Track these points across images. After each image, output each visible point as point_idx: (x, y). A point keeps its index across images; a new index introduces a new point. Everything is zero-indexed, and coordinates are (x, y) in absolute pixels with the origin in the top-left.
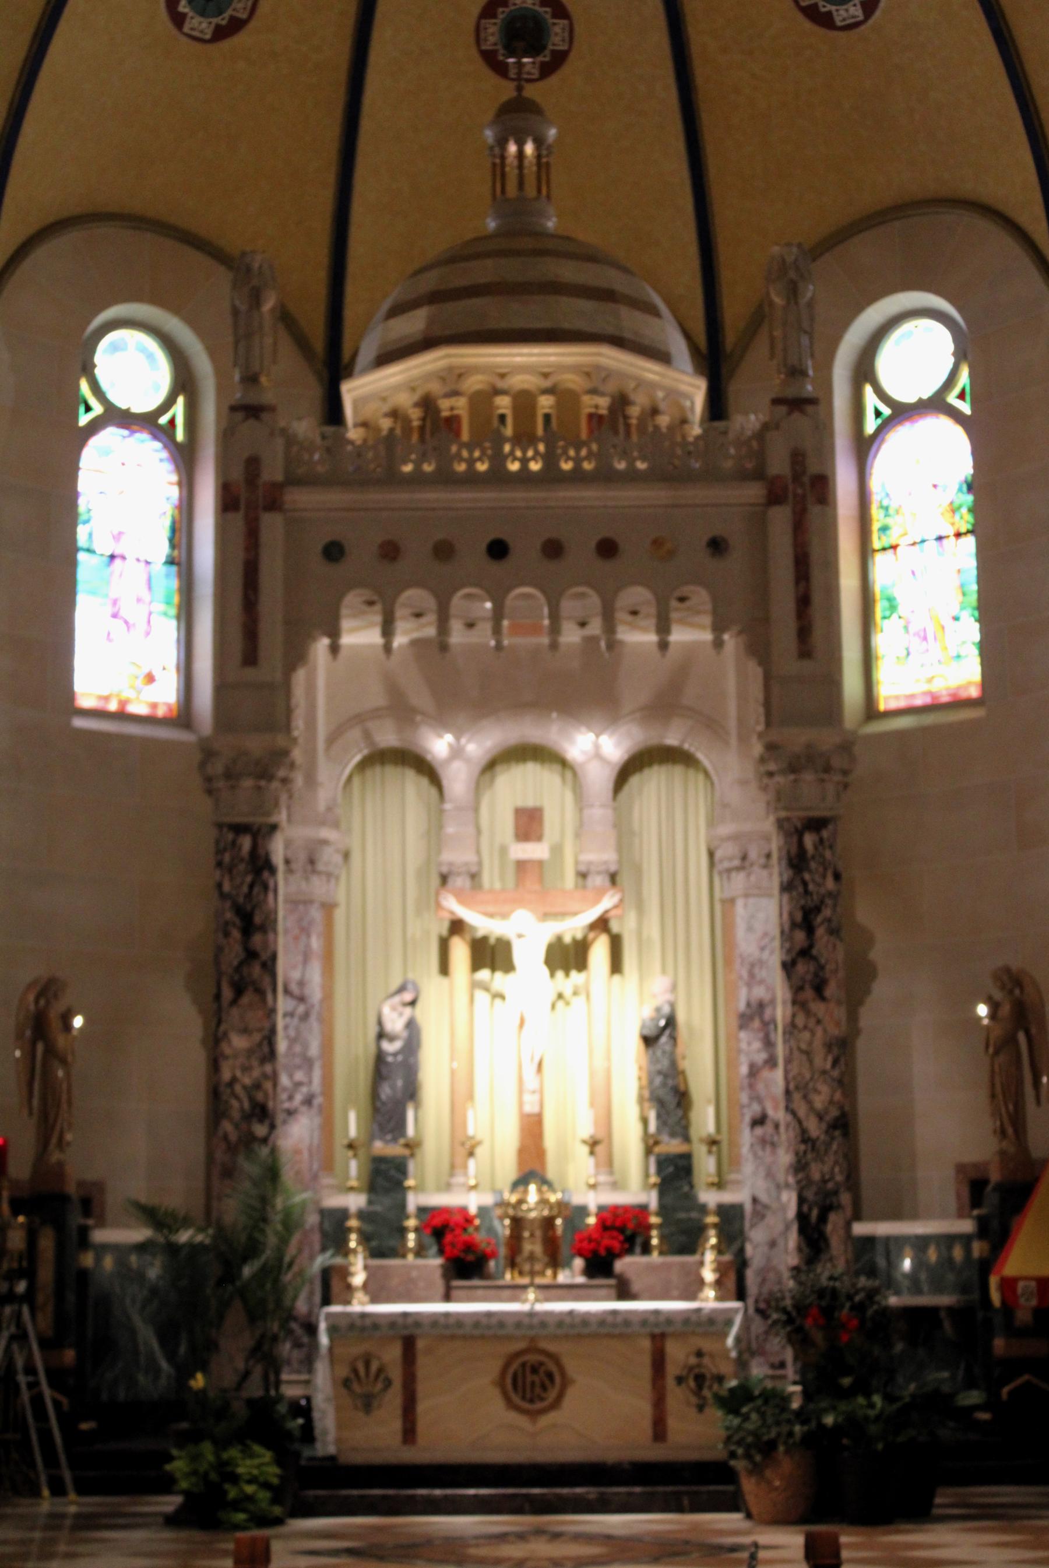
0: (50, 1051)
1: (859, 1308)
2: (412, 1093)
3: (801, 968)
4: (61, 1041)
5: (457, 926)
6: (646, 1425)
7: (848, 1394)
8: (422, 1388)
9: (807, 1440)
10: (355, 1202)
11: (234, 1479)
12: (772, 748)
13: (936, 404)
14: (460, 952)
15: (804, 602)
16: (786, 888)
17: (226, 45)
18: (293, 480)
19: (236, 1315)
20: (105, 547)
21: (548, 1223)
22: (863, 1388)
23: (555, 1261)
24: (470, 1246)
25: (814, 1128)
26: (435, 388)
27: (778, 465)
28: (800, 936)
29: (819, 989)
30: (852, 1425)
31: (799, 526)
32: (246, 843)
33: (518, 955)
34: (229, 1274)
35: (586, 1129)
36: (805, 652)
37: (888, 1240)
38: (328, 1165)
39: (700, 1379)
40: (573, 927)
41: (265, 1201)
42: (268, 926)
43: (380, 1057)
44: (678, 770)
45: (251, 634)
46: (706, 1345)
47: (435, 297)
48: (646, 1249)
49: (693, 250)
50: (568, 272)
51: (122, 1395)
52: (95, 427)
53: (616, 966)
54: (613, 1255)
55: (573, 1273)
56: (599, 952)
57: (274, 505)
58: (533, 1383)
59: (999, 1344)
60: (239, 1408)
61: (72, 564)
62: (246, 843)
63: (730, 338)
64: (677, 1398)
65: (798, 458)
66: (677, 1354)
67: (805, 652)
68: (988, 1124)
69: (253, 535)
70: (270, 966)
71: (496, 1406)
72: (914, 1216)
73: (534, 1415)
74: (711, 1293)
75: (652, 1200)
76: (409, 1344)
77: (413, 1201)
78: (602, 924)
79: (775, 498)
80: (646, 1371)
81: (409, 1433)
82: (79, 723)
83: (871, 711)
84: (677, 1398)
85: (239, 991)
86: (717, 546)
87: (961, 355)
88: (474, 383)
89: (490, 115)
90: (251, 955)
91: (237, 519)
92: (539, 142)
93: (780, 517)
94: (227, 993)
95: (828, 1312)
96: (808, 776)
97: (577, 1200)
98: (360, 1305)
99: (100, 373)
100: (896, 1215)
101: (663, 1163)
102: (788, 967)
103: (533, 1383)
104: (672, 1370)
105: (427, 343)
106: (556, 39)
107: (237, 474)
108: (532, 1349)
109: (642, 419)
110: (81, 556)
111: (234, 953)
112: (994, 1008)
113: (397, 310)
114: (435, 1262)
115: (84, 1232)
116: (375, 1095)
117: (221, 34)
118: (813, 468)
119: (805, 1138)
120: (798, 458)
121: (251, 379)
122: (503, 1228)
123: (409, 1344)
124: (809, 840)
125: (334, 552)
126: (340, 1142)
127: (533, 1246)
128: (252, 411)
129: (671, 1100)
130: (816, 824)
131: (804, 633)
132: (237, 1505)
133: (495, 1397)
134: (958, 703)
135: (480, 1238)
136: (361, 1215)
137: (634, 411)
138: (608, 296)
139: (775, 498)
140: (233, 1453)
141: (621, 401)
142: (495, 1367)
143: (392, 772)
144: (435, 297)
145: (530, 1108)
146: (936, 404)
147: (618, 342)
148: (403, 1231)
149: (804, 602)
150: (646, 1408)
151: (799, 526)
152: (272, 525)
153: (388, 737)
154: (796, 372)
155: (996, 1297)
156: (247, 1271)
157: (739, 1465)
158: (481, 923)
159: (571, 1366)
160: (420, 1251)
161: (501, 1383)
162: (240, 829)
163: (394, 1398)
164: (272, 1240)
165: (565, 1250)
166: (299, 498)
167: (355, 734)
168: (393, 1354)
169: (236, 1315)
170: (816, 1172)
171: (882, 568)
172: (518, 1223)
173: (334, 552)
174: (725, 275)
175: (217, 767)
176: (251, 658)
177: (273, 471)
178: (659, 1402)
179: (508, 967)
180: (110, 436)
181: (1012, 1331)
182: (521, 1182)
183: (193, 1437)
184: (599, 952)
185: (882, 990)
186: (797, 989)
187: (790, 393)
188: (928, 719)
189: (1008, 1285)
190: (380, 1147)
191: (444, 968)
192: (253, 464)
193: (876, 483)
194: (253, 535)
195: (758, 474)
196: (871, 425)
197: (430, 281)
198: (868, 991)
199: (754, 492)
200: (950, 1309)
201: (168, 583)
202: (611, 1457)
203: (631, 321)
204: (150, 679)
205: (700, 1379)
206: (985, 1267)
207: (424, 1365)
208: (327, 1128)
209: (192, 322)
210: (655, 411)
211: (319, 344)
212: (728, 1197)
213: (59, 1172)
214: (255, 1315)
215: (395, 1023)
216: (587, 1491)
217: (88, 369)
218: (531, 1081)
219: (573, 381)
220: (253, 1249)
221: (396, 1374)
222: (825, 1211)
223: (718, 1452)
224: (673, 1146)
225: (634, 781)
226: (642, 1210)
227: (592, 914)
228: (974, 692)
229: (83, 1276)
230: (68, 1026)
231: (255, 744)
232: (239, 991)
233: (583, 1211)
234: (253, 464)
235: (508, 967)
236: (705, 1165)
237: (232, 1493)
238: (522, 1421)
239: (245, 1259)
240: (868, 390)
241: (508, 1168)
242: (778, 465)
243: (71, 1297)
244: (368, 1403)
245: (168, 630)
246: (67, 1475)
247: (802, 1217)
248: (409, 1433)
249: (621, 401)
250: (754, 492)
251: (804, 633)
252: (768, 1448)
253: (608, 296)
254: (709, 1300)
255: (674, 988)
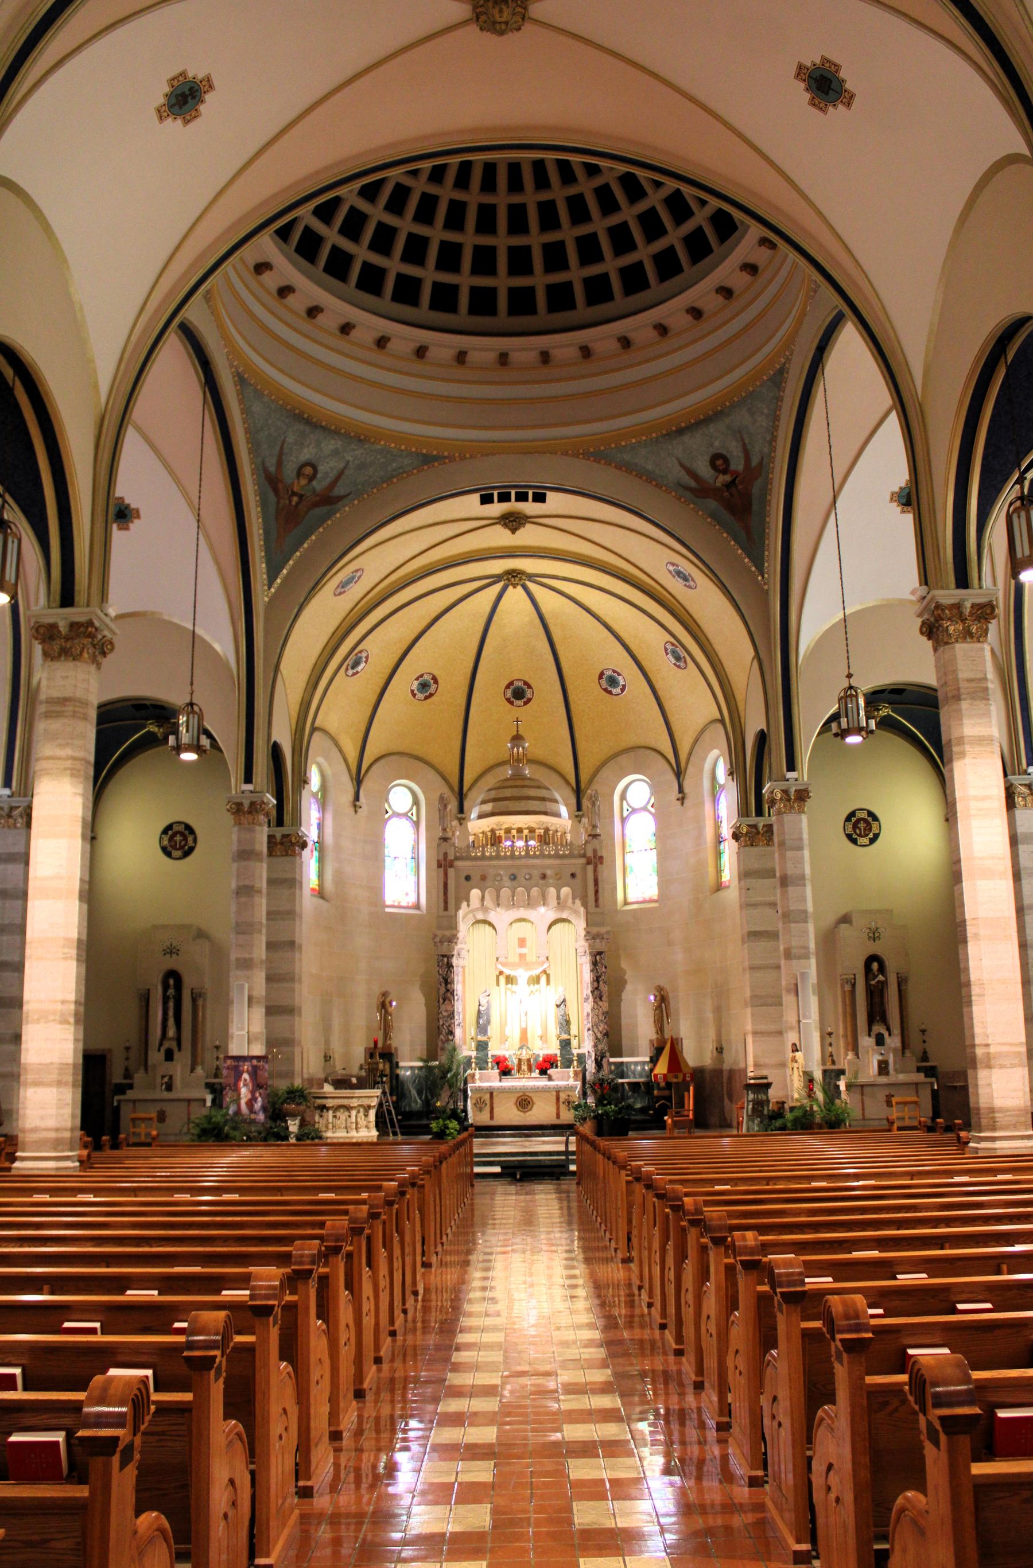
0: (386, 1012)
1: (609, 1083)
2: (488, 1022)
3: (596, 992)
4: (389, 1010)
5: (501, 973)
6: (555, 1115)
7: (605, 1105)
8: (495, 1106)
9: (595, 1117)
10: (474, 1054)
11: (448, 1128)
12: (588, 933)
13: (645, 809)
14: (502, 979)
15: (597, 892)
16: (592, 971)
17: (428, 701)
18: (457, 858)
19: (446, 1086)
20: (393, 855)
21: (529, 1060)
22: (610, 1104)
23: (530, 1070)
24: (507, 1067)
25: (599, 1036)
26: (495, 827)
27: (590, 854)
28: (596, 984)
29: (601, 999)
30: (606, 1113)
31: (595, 871)
32: (445, 960)
33: (520, 980)
34: (444, 1076)
35: (540, 1033)
36: (597, 906)
37: (627, 1063)
38: (465, 1043)
39: (569, 1102)
40: (536, 972)
41: (452, 1057)
42: (452, 982)
43: (479, 1011)
44: (567, 924)
45: (446, 902)
46: (570, 1093)
47: (494, 800)
48: (557, 1067)
49: (571, 758)
50: (532, 792)
51: (407, 1109)
52: (389, 818)
53: (548, 983)
54: (547, 1069)
55: (536, 1073)
56: (543, 979)
57: (451, 866)
58: (699, 1386)
59: (656, 1092)
60: (448, 1110)
61: (384, 861)
62: (445, 960)
63: (583, 786)
64: (563, 1107)
65: (595, 851)
66: (563, 1096)
67: (597, 906)
68: (654, 1030)
69: (446, 874)
70: (452, 993)
71: (515, 1110)
72: (638, 1056)
73: (525, 1112)
74: (572, 1080)
75: (558, 1052)
76: (491, 1094)
77: (490, 1054)
78: (544, 972)
79: (589, 863)
80: (555, 1101)
81: (492, 1117)
82: (387, 910)
83: (626, 903)
84: (563, 1107)
85: (444, 1000)
86: (573, 875)
87: (652, 794)
88: (505, 826)
89: (509, 738)
90: (448, 990)
91: (441, 870)
92: (523, 748)
93: (590, 868)
94: (441, 1001)
95: (601, 1085)
96: (598, 941)
97: (536, 1052)
98: (478, 1084)
99: (391, 801)
100: (632, 1055)
101: (561, 1042)
102: (592, 992)
103: (699, 1386)
104: (561, 1100)
105: (493, 814)
106: (528, 694)
107: (441, 857)
108: (524, 1095)
109: (553, 835)
110: (386, 858)
111: (443, 990)
112: (656, 996)
113: (483, 802)
114: (497, 1071)
115: (397, 1063)
116: (478, 1022)
117: (426, 698)
118: (599, 854)
119: (597, 1038)
120: (595, 851)
121: (444, 830)
122: (516, 1061)
123: (491, 1094)
124: (598, 958)
125: (468, 878)
126: (468, 1038)
127: (524, 1067)
128: (445, 839)
129: (564, 1024)
130: (600, 953)
131: (597, 900)
132: (448, 1135)
133: (515, 1108)
134: (651, 901)
135: (509, 1063)
136: (476, 1058)
137: (551, 832)
138: (543, 799)
139: (589, 863)
140: (448, 1122)
141: (547, 830)
142: (514, 1100)
143: (482, 926)
144: (494, 800)
145: (524, 1026)
146: (645, 809)
147: (546, 813)
148: (487, 1062)
149: (597, 892)
150: (555, 1110)
151: (595, 871)
152: (451, 872)
153: (480, 916)
154: (594, 827)
155: (115, 1104)
156: (449, 1075)
157: (578, 1124)
158: (507, 971)
159: (534, 1099)
160: (492, 1069)
161: (516, 1104)
162: (443, 956)
163: (488, 1109)
164: (455, 1067)
165: (533, 1068)
166: (458, 863)
167: (471, 916)
168: (488, 1096)
169: (446, 1086)
170: (600, 1047)
171: (628, 857)
172: (520, 1060)
173: (468, 878)
174: (581, 766)
175: (437, 939)
176: (446, 909)
177: (451, 857)
178: (558, 1109)
179: (517, 984)
180: (394, 820)
181: (659, 1089)
182: (521, 1048)
183: (437, 1118)
184: (543, 979)
185: (629, 987)
186: (595, 998)
187: (593, 833)
188: (642, 906)
189: (656, 1076)
190: (480, 1038)
191: (498, 984)
192: (446, 855)
193: (627, 831)
194: (446, 874)
195: (584, 856)
196: (625, 813)
197: (493, 794)
198: (624, 988)
199: (583, 861)
200: (643, 1083)
201: (412, 864)
202: (545, 1123)
203: (550, 806)
204: (407, 894)
205: (569, 1102)
206: (652, 1070)
207: (495, 1098)
208: (464, 1032)
209: (418, 784)
210: (557, 831)
211: (456, 788)
212: (580, 1051)
213: (390, 1046)
214: (451, 1086)
215: (484, 1002)
216: (540, 1132)
217: (387, 800)
218: (524, 1018)
219: (533, 825)
220: (449, 1070)
221: (488, 1102)
222: (602, 1057)
223: (572, 1122)
224: (565, 1036)
225: (553, 928)
226: (556, 1055)
227: (541, 969)
228: (656, 898)
229: (397, 1076)
230: (391, 1005)
231: (447, 933)
232: (444, 1000)
233: (538, 1055)
234: (446, 855)
235: (517, 984)
236: (574, 1043)
237: (448, 1132)
238: (522, 1114)
239: (448, 1072)
240: (625, 802)
241: (517, 1043)
242: (590, 854)
243: (394, 1082)
244: (481, 1110)
245: (413, 879)
246: (398, 1130)
247: (596, 1059)
248: (492, 1117)
249: (547, 830)
250: (583, 861)
251: (597, 900)
252: (584, 1119)
253: (543, 799)
254: (571, 1082)
255: (565, 990)
